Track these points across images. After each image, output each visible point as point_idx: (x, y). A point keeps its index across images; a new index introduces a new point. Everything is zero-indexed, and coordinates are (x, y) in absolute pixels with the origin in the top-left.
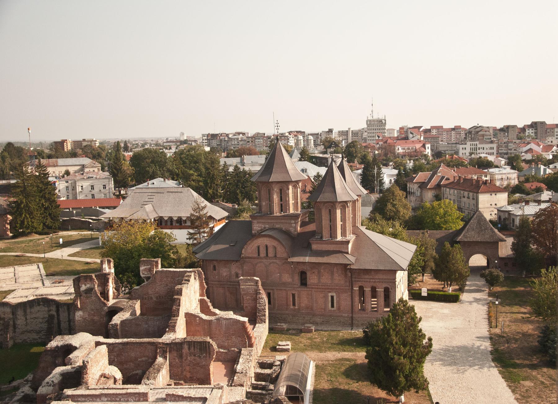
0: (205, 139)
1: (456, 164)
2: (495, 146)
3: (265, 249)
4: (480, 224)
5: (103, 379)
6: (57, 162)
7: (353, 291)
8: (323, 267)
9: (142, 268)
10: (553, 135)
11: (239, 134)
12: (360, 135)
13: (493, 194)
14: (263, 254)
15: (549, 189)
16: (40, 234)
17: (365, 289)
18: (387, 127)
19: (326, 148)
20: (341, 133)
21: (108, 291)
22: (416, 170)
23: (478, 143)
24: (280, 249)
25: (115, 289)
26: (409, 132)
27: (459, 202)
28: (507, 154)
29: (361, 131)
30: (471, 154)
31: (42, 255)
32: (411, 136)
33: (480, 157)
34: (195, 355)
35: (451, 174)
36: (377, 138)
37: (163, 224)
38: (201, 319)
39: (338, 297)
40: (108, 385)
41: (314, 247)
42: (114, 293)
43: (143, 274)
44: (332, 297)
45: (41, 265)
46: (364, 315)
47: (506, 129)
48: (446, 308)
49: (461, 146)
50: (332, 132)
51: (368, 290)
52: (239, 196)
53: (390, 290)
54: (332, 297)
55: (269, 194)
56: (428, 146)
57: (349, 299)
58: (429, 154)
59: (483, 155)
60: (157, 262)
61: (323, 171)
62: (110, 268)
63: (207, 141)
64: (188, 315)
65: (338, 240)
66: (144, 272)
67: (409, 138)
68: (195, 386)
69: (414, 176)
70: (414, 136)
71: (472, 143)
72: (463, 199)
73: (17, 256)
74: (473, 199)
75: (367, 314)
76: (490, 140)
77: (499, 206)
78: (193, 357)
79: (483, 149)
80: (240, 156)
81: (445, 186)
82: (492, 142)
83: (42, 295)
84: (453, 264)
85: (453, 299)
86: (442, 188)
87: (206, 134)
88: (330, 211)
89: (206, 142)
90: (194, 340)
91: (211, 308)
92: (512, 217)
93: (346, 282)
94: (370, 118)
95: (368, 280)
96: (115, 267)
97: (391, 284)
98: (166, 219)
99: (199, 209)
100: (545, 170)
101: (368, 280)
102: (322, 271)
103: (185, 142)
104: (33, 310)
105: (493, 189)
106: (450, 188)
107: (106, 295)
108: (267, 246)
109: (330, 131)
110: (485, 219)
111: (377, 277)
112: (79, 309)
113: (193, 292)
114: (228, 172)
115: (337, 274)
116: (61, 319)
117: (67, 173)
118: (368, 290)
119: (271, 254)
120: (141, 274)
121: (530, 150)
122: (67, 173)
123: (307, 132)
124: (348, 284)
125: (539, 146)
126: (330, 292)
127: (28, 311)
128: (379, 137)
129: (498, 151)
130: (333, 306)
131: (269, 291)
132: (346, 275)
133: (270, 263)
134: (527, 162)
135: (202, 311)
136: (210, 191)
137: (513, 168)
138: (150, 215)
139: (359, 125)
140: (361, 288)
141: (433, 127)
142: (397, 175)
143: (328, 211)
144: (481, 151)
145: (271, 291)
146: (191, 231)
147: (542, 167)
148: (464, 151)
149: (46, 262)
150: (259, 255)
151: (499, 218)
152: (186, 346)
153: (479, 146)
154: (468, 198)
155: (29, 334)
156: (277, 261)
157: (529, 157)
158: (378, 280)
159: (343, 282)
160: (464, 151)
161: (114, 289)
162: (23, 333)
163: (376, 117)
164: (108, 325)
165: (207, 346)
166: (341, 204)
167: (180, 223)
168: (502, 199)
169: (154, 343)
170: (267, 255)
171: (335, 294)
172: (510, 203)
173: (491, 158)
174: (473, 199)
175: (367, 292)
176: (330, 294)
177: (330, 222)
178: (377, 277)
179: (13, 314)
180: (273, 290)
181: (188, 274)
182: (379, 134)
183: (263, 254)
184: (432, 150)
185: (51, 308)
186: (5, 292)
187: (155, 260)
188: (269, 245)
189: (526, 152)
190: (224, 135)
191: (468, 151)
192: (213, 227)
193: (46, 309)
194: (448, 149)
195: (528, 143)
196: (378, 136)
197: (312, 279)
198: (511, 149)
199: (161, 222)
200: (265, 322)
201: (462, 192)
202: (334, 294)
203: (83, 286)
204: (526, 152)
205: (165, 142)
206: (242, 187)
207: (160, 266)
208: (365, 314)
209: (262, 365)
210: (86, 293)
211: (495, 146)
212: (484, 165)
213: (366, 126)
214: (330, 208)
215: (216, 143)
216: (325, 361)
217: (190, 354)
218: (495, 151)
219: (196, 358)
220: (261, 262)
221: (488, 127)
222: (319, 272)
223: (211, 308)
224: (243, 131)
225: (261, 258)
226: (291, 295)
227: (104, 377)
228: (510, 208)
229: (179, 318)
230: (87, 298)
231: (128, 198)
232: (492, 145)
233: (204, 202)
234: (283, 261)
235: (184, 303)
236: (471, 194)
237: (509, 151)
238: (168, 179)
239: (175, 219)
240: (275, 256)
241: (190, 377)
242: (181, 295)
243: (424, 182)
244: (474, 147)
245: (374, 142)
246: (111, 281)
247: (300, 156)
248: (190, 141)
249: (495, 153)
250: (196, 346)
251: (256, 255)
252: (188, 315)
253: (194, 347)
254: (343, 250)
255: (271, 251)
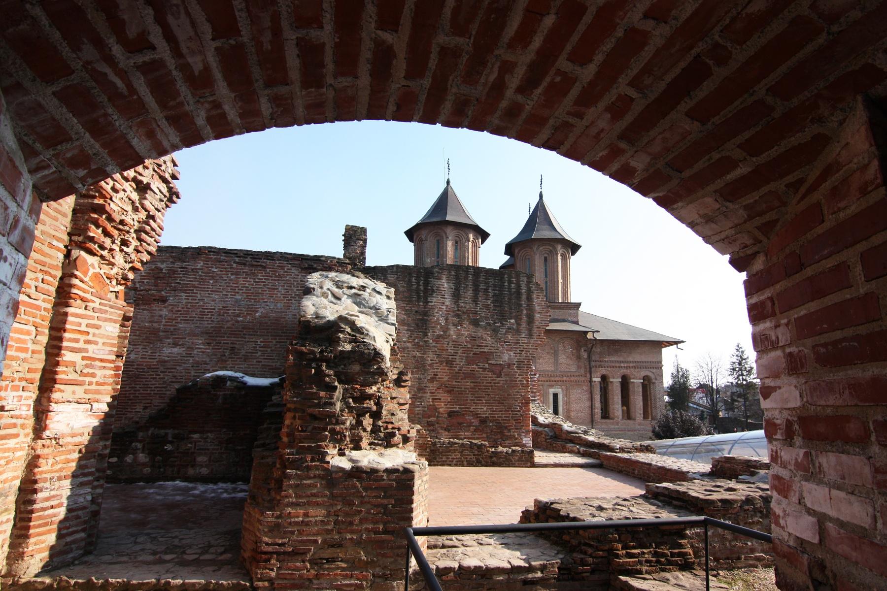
7: (593, 384)
34: (475, 323)
39: (567, 395)
44: (555, 396)
46: (613, 427)
54: (555, 396)
57: (585, 399)
75: (617, 424)
78: (467, 330)
88: (546, 259)
93: (579, 367)
95: (617, 365)
101: (617, 365)
115: (563, 356)
124: (582, 371)
126: (552, 386)
140: (604, 378)
143: (543, 258)
158: (634, 364)
159: (573, 369)
165: (524, 290)
171: (560, 390)
175: (615, 384)
176: (552, 391)
177: (546, 276)
178: (631, 359)
202: (558, 390)
208: (613, 424)
214: (546, 255)
216: (857, 363)
217: (459, 315)
219: (480, 333)
231: (33, 575)
241: (451, 414)
250: (482, 286)
253: (476, 290)
254: (569, 319)
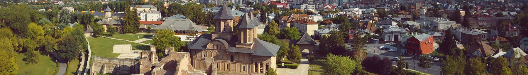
1: (299, 13)
4: (306, 37)
6: (141, 6)
8: (240, 54)
10: (335, 2)
13: (313, 25)
15: (334, 23)
16: (132, 33)
19: (247, 5)
22: (283, 15)
23: (308, 4)
27: (300, 28)
28: (319, 9)
30: (305, 9)
31: (132, 41)
33: (309, 10)
35: (297, 17)
37: (178, 32)
38: (188, 73)
41: (237, 46)
42: (154, 59)
45: (131, 45)
48: (292, 71)
49: (301, 6)
52: (210, 23)
56: (288, 5)
58: (289, 8)
59: (310, 9)
60: (172, 49)
61: (243, 14)
62: (154, 49)
64: (182, 71)
65: (247, 43)
68: (225, 35)
69: (282, 17)
71: (305, 4)
72: (301, 27)
73: (123, 41)
74: (305, 27)
77: (315, 30)
81: (294, 21)
83: (130, 57)
85: (295, 67)
88: (244, 31)
92: (320, 34)
93: (250, 60)
98: (179, 31)
99: (192, 28)
100: (332, 16)
102: (240, 56)
104: (126, 62)
105: (313, 23)
108: (217, 45)
110: (309, 35)
111: (263, 59)
112: (142, 65)
113: (185, 62)
116: (135, 67)
117: (144, 11)
121: (327, 8)
122: (144, 11)
125: (330, 6)
127: (124, 62)
129: (315, 7)
130: (244, 70)
132: (250, 58)
134: (326, 12)
135: (189, 70)
136: (198, 21)
137: (321, 15)
138: (173, 29)
142: (275, 16)
144: (309, 8)
145: (218, 63)
146: (188, 36)
147: (331, 15)
148: (302, 8)
149: (132, 44)
151: (315, 34)
154: (303, 26)
155: (124, 71)
157: (327, 10)
160: (302, 8)
162: (122, 71)
167: (184, 33)
168: (316, 27)
172: (319, 29)
173: (313, 11)
176: (243, 65)
179: (119, 63)
180: (219, 63)
184: (290, 6)
185: (132, 62)
186: (119, 54)
188: (218, 44)
191: (304, 8)
192: (198, 35)
193: (130, 63)
194: (296, 6)
195: (327, 5)
198: (320, 7)
199: (177, 32)
202: (245, 65)
203: (143, 55)
206: (211, 19)
207: (173, 50)
210: (144, 59)
211: (314, 6)
212: (310, 13)
218: (314, 8)
222: (239, 56)
228: (319, 31)
229: (179, 72)
230: (144, 60)
233: (194, 25)
234: (224, 51)
235: (181, 66)
236: (304, 25)
239: (182, 31)
240: (221, 49)
242: (180, 63)
243: (286, 20)
247: (235, 8)
249: (314, 9)
252: (182, 71)
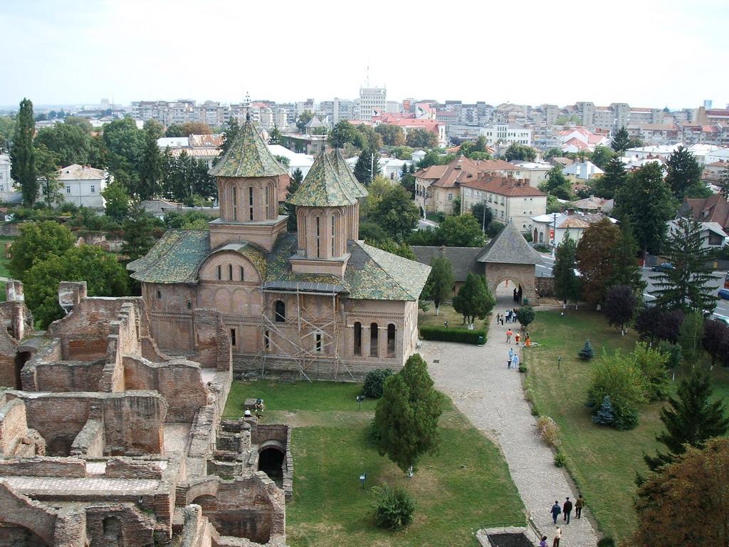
0: (137, 109)
2: (529, 131)
3: (229, 269)
5: (20, 445)
9: (61, 294)
11: (184, 102)
12: (350, 109)
13: (528, 199)
14: (225, 277)
17: (362, 326)
18: (388, 99)
20: (325, 105)
21: (18, 326)
23: (507, 126)
24: (249, 270)
25: (27, 322)
26: (417, 108)
29: (355, 104)
32: (418, 113)
36: (374, 114)
40: (28, 454)
41: (295, 268)
43: (63, 302)
47: (544, 110)
50: (312, 103)
51: (366, 328)
53: (396, 328)
55: (235, 194)
62: (18, 294)
63: (138, 112)
66: (64, 300)
67: (417, 116)
70: (424, 112)
75: (365, 360)
76: (523, 124)
79: (515, 135)
80: (187, 135)
82: (525, 126)
84: (475, 285)
86: (462, 188)
87: (138, 103)
89: (137, 114)
90: (137, 395)
91: (157, 350)
94: (365, 86)
96: (24, 292)
97: (397, 320)
103: (108, 112)
106: (472, 188)
107: (15, 331)
108: (231, 266)
109: (310, 102)
114: (171, 157)
118: (366, 328)
119: (236, 276)
120: (60, 302)
123: (279, 101)
128: (376, 113)
129: (532, 138)
131: (233, 327)
133: (235, 290)
139: (350, 94)
141: (448, 103)
145: (236, 328)
150: (242, 279)
152: (127, 404)
153: (509, 131)
156: (246, 287)
161: (26, 324)
163: (372, 86)
164: (20, 372)
165: (156, 403)
166: (334, 210)
169: (84, 398)
170: (231, 279)
174: (502, 204)
181: (125, 304)
182: (377, 109)
183: (225, 277)
187: (79, 283)
189: (569, 142)
190: (164, 104)
196: (375, 112)
197: (292, 312)
200: (228, 370)
201: (488, 195)
204: (569, 142)
205: (80, 112)
209: (227, 428)
211: (529, 131)
213: (359, 97)
215: (151, 114)
220: (221, 288)
221: (521, 107)
223: (157, 350)
224: (191, 99)
225: (223, 282)
226: (236, 344)
227: (23, 443)
232: (525, 131)
234: (253, 288)
237: (547, 140)
238: (89, 167)
244: (502, 132)
245: (370, 119)
246: (21, 312)
248: (115, 111)
250: (140, 403)
251: (215, 279)
253: (138, 405)
255: (236, 273)
